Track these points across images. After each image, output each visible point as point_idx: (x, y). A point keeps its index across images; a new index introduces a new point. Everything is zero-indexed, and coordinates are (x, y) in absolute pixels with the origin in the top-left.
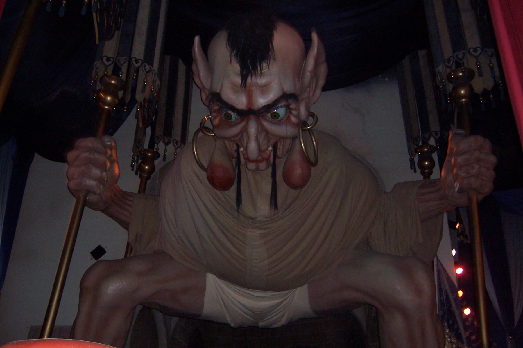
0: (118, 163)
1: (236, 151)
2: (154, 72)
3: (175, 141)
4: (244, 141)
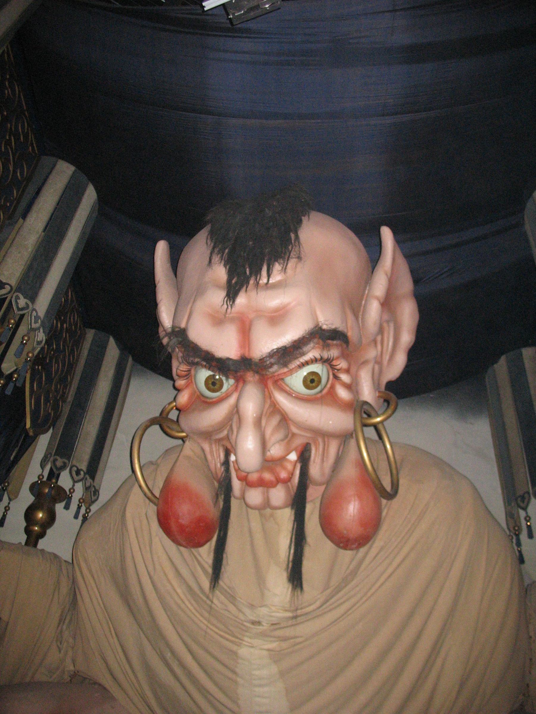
0: (7, 491)
2: (34, 313)
3: (75, 469)
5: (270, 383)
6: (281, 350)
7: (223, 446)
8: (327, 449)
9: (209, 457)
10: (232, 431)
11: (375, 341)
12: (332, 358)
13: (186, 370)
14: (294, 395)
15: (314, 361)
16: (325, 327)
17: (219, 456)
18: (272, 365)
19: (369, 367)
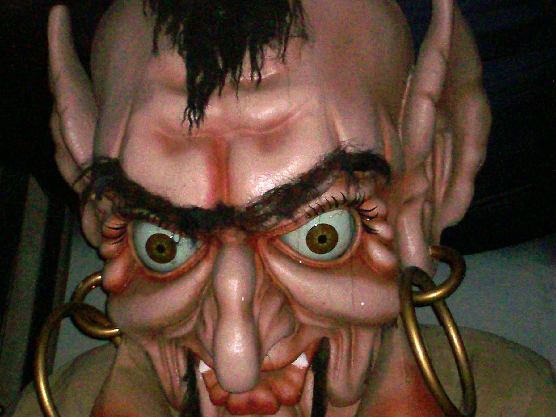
1: (185, 379)
4: (205, 330)
5: (261, 243)
6: (281, 191)
7: (184, 347)
8: (356, 348)
9: (159, 367)
10: (204, 323)
11: (423, 165)
12: (362, 199)
13: (118, 227)
14: (300, 262)
15: (334, 205)
16: (350, 150)
17: (178, 365)
18: (268, 215)
19: (417, 208)
